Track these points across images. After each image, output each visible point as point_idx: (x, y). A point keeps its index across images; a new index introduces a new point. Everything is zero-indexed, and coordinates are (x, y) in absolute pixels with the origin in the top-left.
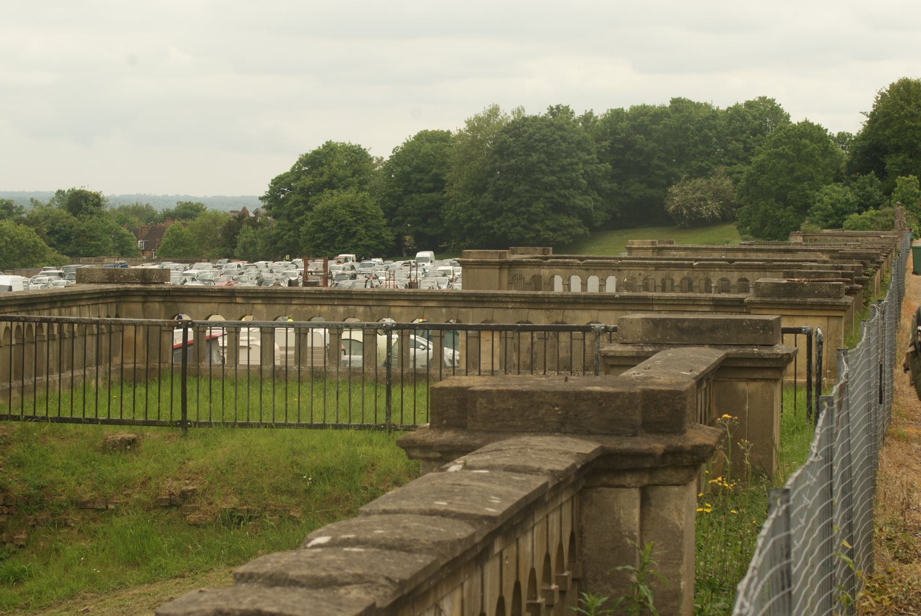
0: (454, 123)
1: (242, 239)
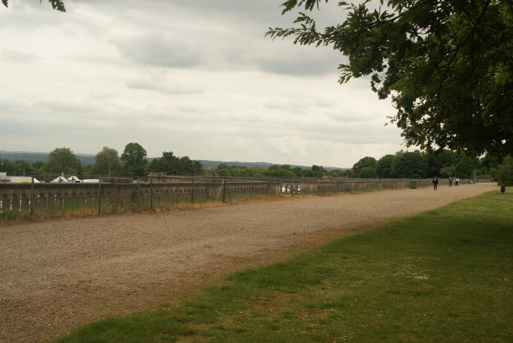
0: (393, 153)
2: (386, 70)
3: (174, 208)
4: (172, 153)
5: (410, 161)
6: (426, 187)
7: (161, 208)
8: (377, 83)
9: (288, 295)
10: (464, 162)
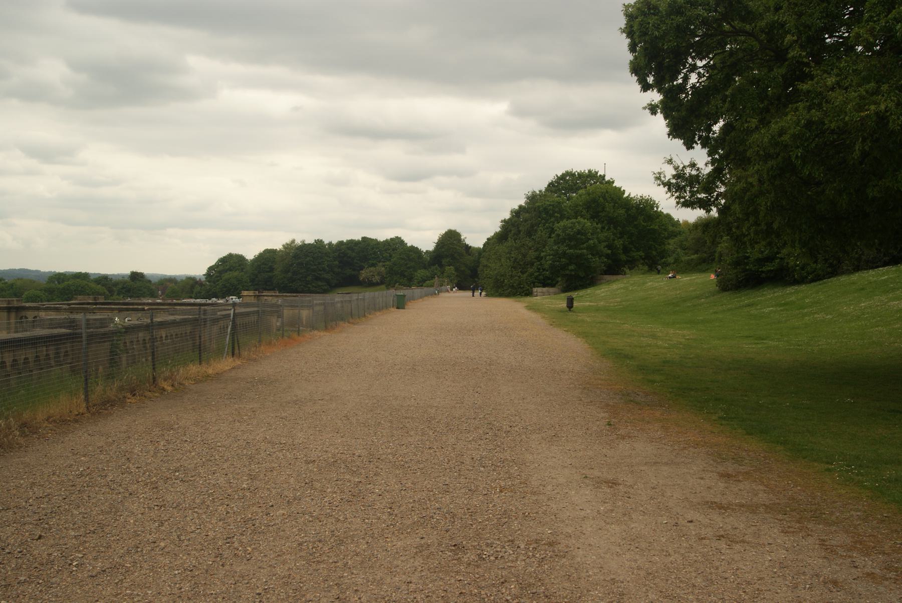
0: (278, 246)
1: (195, 291)
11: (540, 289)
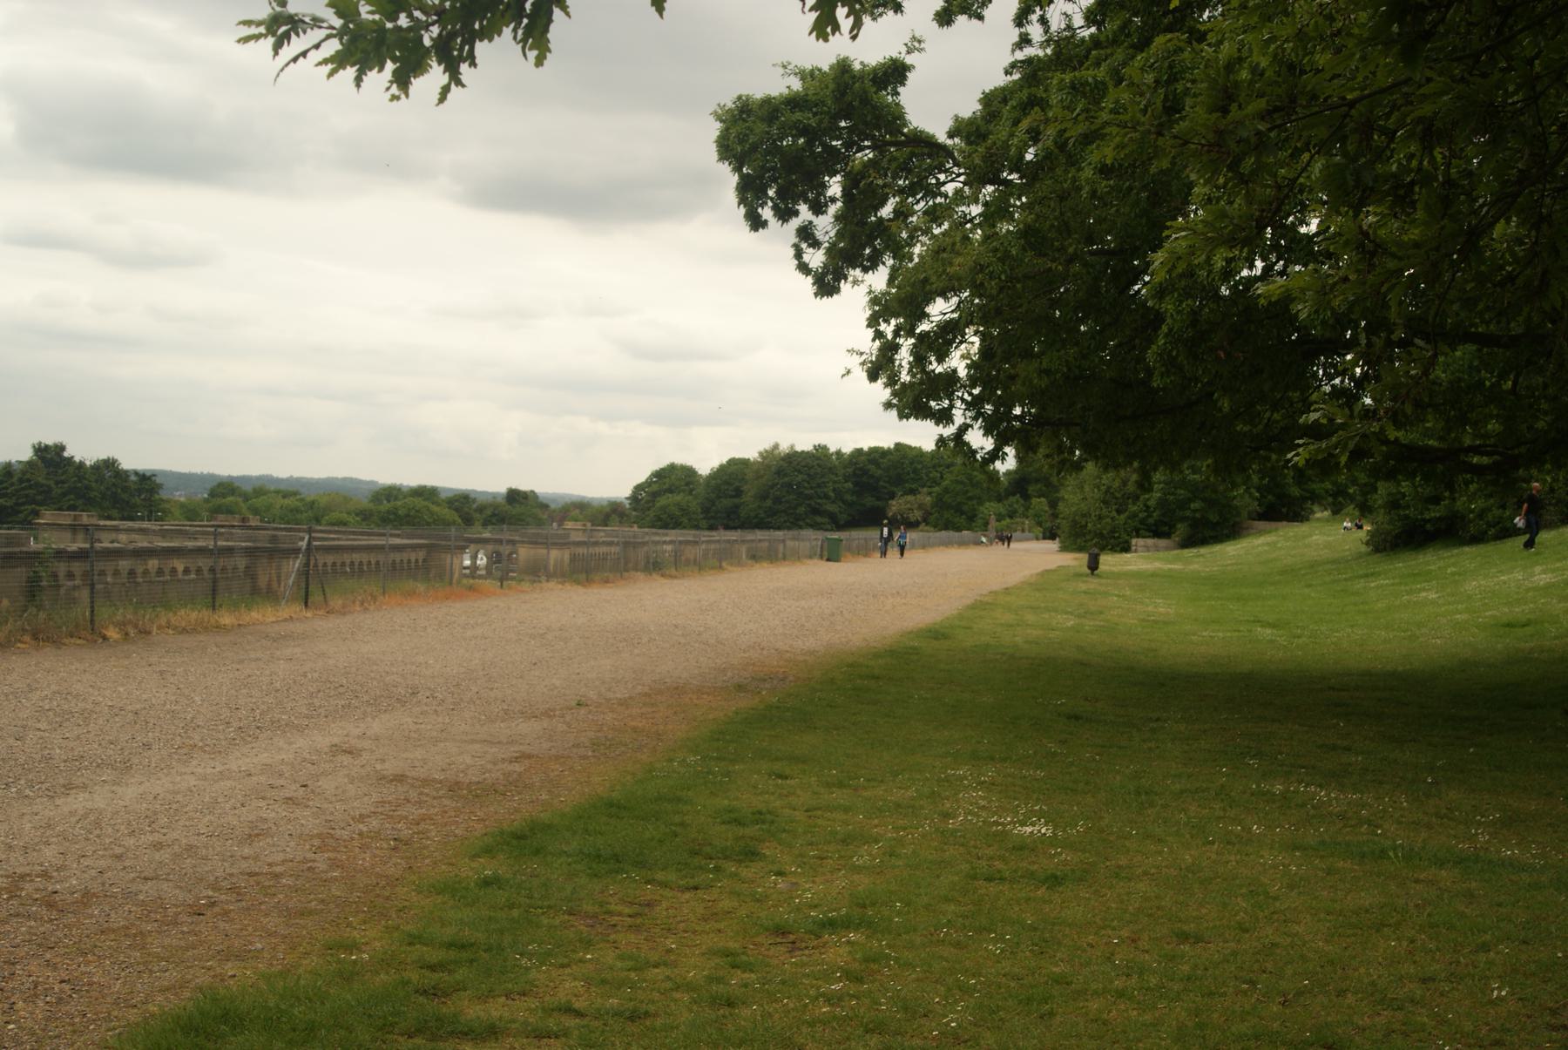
0: (751, 453)
2: (833, 209)
3: (160, 627)
4: (63, 448)
5: (800, 478)
6: (866, 555)
7: (121, 625)
8: (811, 250)
9: (687, 896)
10: (957, 482)
11: (1141, 542)
